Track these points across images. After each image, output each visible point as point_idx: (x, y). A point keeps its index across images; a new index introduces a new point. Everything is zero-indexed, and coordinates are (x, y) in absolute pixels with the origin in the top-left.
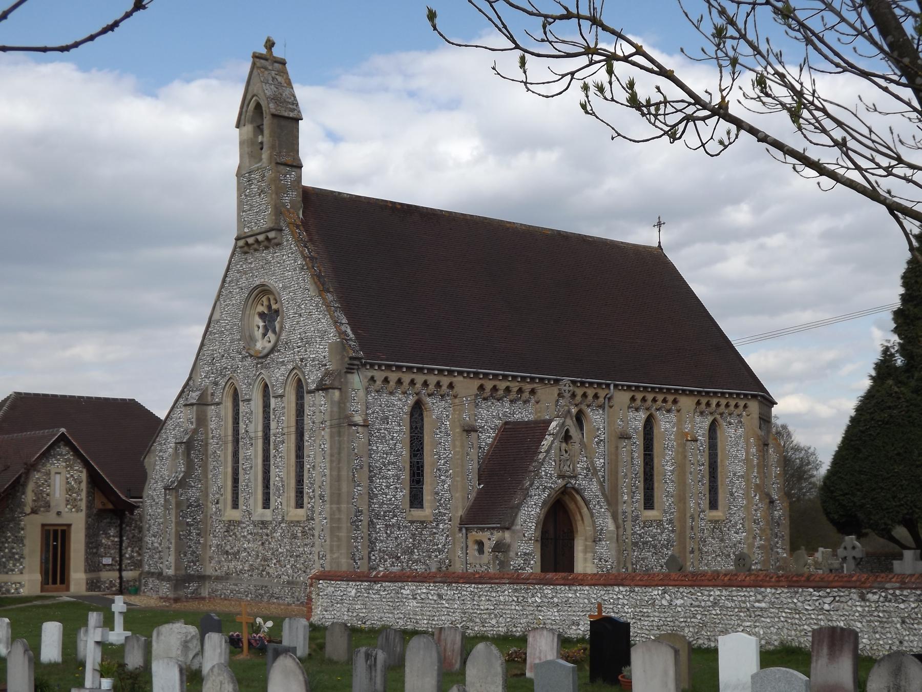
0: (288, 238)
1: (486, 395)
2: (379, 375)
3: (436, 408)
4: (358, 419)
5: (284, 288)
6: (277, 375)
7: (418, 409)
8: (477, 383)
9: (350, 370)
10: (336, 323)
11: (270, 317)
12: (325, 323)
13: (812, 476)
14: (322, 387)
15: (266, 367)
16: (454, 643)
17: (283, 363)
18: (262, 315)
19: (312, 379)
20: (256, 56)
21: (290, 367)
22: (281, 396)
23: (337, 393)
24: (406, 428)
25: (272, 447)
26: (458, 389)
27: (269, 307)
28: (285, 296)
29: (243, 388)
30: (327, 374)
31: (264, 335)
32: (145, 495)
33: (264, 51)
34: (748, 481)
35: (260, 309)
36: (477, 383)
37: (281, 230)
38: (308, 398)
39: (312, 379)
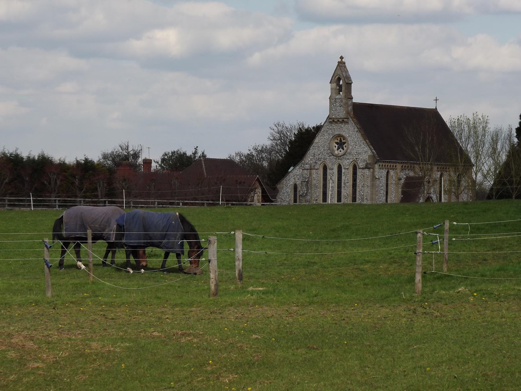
0: (351, 121)
1: (402, 170)
2: (381, 164)
3: (392, 173)
4: (377, 177)
5: (349, 136)
6: (346, 163)
7: (388, 172)
8: (401, 165)
9: (376, 163)
10: (371, 150)
11: (341, 145)
12: (367, 148)
13: (148, 163)
14: (367, 167)
15: (341, 159)
16: (239, 265)
17: (348, 159)
18: (337, 143)
19: (361, 165)
20: (339, 62)
21: (351, 160)
22: (348, 169)
23: (372, 170)
24: (385, 179)
25: (342, 184)
26: (397, 167)
27: (341, 141)
28: (349, 139)
29: (329, 165)
30: (367, 164)
31: (338, 150)
32: (277, 198)
33: (340, 60)
34: (468, 195)
35: (337, 141)
36: (401, 165)
37: (348, 119)
38: (359, 172)
39: (361, 165)
